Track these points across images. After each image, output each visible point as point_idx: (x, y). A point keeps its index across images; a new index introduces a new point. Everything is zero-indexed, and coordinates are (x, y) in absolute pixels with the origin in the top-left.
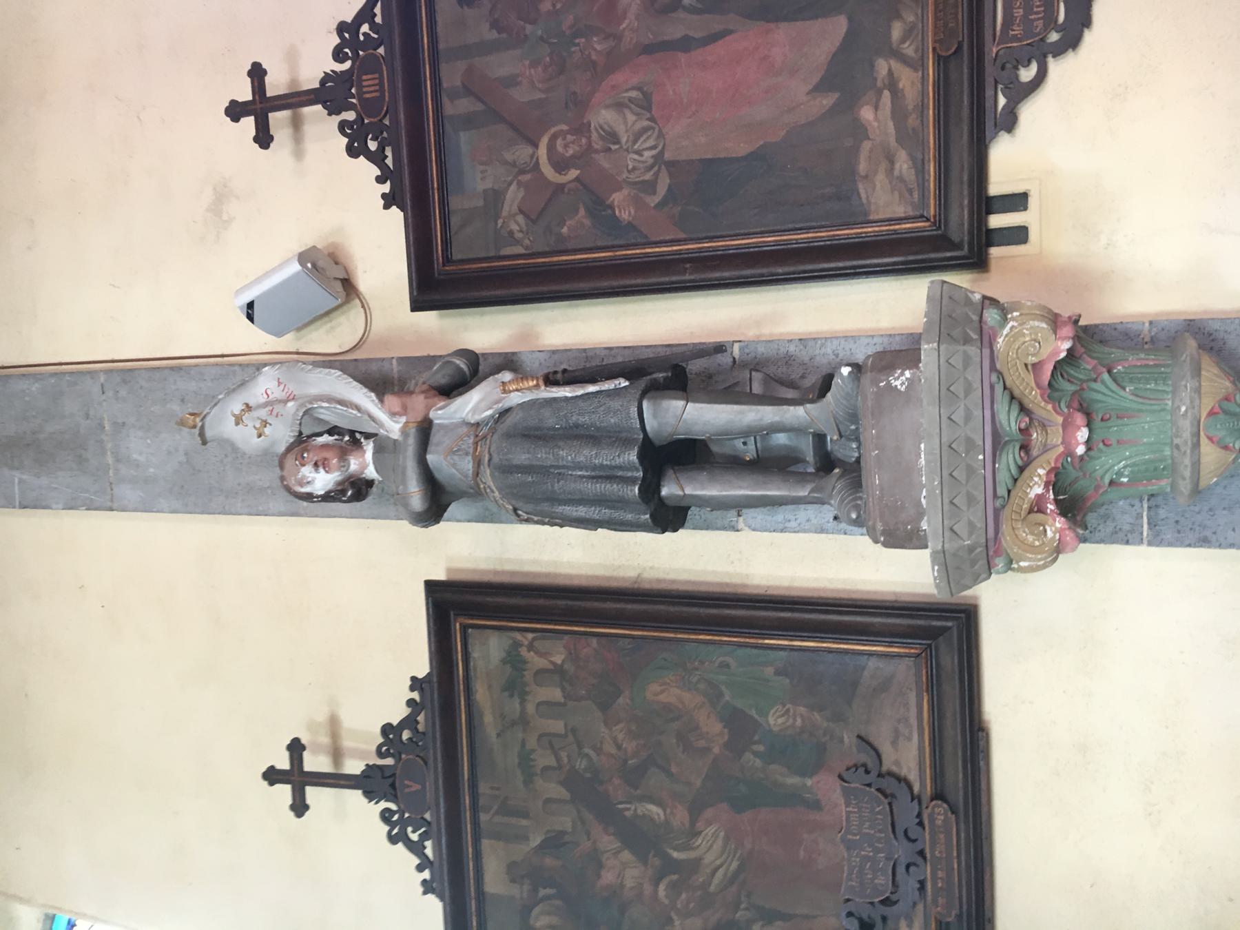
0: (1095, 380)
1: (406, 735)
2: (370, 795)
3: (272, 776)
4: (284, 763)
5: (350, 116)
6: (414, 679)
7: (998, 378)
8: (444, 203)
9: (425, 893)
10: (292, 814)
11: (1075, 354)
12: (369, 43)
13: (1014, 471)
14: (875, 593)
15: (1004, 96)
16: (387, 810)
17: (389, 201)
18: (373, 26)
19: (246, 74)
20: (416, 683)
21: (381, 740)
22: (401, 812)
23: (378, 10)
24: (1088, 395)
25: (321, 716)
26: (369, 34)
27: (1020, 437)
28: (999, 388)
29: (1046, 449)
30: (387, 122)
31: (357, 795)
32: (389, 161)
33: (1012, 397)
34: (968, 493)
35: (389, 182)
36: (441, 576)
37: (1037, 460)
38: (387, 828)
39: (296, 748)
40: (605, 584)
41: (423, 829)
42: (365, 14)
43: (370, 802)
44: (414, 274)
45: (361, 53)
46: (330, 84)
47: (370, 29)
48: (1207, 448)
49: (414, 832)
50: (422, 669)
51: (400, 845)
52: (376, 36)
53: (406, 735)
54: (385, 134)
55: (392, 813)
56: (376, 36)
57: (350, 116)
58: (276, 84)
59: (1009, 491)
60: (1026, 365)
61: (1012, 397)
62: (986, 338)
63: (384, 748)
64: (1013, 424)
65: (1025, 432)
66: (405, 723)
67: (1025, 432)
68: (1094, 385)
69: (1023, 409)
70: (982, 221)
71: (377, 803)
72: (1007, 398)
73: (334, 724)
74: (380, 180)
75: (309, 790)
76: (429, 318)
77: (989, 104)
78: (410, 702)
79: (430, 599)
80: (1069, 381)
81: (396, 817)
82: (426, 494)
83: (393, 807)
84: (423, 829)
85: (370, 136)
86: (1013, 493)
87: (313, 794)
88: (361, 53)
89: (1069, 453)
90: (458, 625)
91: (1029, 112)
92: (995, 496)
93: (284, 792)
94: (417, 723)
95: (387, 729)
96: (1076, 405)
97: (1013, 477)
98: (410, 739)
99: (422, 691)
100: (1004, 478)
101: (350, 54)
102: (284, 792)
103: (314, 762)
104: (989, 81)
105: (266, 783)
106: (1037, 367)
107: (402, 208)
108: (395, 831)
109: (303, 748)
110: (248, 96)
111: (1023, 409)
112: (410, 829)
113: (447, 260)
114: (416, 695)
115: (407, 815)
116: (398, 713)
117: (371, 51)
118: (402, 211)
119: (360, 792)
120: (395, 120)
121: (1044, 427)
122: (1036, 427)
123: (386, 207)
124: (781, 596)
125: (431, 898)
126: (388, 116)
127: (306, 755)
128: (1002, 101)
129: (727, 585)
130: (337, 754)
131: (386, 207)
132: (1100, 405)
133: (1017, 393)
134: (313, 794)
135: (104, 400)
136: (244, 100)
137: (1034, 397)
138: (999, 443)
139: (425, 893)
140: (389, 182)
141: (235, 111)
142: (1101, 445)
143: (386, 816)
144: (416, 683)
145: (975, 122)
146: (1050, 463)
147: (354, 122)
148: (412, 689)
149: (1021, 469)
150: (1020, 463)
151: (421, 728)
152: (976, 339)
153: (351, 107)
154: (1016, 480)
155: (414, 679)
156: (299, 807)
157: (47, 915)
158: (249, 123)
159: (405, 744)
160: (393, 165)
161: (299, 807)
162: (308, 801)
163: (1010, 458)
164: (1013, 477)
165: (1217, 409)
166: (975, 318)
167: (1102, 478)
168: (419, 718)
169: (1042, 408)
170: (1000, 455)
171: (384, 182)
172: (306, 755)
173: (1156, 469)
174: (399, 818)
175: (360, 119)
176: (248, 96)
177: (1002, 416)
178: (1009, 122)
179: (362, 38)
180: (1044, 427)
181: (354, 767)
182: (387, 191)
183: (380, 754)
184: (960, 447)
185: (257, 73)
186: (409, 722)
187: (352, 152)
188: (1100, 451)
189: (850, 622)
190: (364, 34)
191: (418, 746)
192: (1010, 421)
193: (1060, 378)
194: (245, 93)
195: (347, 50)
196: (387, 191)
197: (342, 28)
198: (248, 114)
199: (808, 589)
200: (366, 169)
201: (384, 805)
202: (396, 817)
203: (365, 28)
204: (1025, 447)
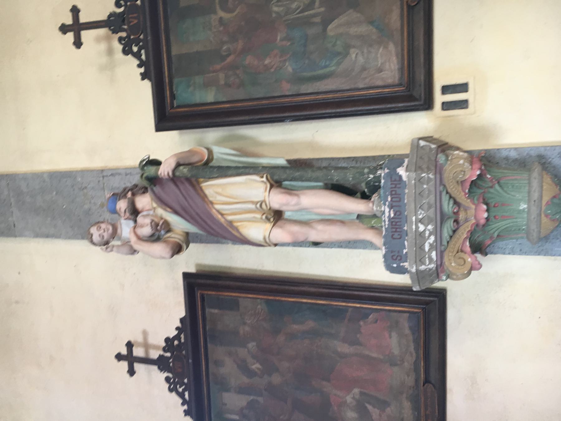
1: (176, 342)
2: (161, 369)
3: (119, 357)
4: (124, 352)
5: (124, 34)
13: (451, 233)
14: (345, 278)
17: (144, 76)
22: (174, 378)
24: (488, 195)
29: (466, 220)
30: (142, 37)
31: (155, 368)
32: (143, 57)
33: (451, 197)
36: (192, 270)
39: (130, 345)
40: (272, 277)
43: (161, 372)
48: (544, 220)
49: (180, 387)
53: (176, 342)
57: (124, 34)
59: (448, 242)
61: (451, 197)
62: (439, 170)
63: (166, 348)
65: (456, 213)
66: (175, 338)
68: (492, 190)
69: (456, 203)
72: (448, 196)
73: (145, 334)
74: (139, 66)
82: (351, 283)
87: (138, 366)
93: (70, 36)
95: (167, 340)
96: (481, 200)
102: (124, 365)
103: (138, 352)
106: (462, 182)
107: (150, 79)
108: (172, 386)
111: (456, 203)
112: (178, 386)
113: (172, 107)
116: (173, 333)
120: (146, 37)
121: (465, 210)
123: (143, 79)
124: (345, 280)
127: (134, 349)
129: (256, 270)
131: (185, 415)
133: (453, 195)
134: (138, 366)
137: (462, 197)
138: (443, 217)
141: (64, 29)
143: (167, 379)
149: (454, 231)
151: (183, 340)
153: (124, 30)
154: (451, 237)
156: (132, 372)
158: (70, 36)
161: (132, 372)
163: (449, 225)
171: (141, 67)
172: (134, 348)
173: (519, 230)
175: (128, 37)
180: (465, 210)
181: (154, 354)
185: (75, 11)
186: (177, 337)
189: (383, 296)
192: (448, 207)
194: (69, 21)
198: (70, 31)
199: (314, 275)
200: (133, 62)
201: (166, 374)
204: (456, 221)
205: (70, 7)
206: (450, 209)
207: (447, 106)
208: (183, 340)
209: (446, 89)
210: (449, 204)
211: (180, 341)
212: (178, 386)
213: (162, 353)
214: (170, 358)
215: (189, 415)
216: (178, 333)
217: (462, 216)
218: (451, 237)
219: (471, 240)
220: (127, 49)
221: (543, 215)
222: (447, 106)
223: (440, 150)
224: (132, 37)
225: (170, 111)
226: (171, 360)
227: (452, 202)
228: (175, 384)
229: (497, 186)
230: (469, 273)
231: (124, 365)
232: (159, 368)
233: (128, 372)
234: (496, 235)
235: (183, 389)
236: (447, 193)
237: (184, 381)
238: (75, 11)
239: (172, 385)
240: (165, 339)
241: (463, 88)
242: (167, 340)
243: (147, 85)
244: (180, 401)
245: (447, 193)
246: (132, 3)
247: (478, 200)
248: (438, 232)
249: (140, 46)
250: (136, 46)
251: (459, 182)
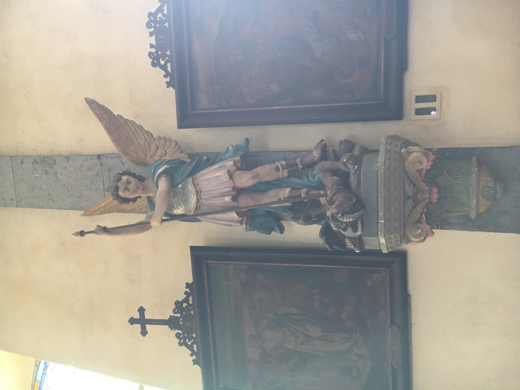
1: (185, 305)
3: (132, 321)
4: (137, 316)
6: (187, 284)
8: (206, 109)
9: (194, 364)
12: (162, 22)
16: (178, 333)
17: (169, 84)
18: (164, 15)
19: (144, 337)
20: (188, 285)
22: (184, 334)
23: (165, 8)
26: (161, 18)
35: (169, 77)
36: (200, 243)
38: (178, 340)
42: (160, 10)
46: (172, 83)
47: (162, 16)
49: (189, 341)
50: (190, 280)
52: (164, 19)
53: (185, 305)
54: (167, 58)
56: (164, 19)
58: (148, 316)
59: (409, 216)
67: (415, 194)
69: (415, 185)
71: (174, 330)
74: (191, 355)
78: (186, 293)
81: (182, 336)
85: (161, 59)
87: (148, 327)
88: (158, 25)
89: (430, 202)
90: (204, 263)
92: (404, 218)
93: (138, 327)
97: (410, 210)
98: (186, 307)
107: (174, 88)
108: (182, 341)
110: (147, 317)
111: (415, 185)
112: (187, 340)
114: (188, 290)
115: (186, 335)
116: (181, 297)
118: (174, 89)
125: (196, 366)
126: (169, 50)
134: (148, 327)
135: (52, 180)
136: (141, 330)
138: (406, 198)
139: (194, 364)
140: (169, 77)
143: (178, 336)
144: (188, 285)
146: (424, 205)
147: (155, 53)
148: (186, 288)
151: (191, 302)
154: (411, 212)
155: (187, 284)
156: (144, 333)
157: (45, 362)
161: (144, 333)
163: (410, 203)
164: (410, 210)
166: (399, 151)
168: (164, 8)
169: (422, 185)
174: (183, 336)
175: (157, 52)
176: (147, 317)
177: (407, 186)
179: (158, 19)
182: (168, 81)
183: (174, 312)
185: (141, 310)
186: (186, 300)
187: (154, 65)
190: (159, 18)
192: (410, 190)
195: (152, 23)
196: (168, 81)
197: (150, 15)
201: (177, 331)
202: (182, 336)
203: (160, 15)
207: (419, 112)
208: (191, 302)
209: (419, 99)
211: (188, 303)
212: (187, 340)
214: (180, 318)
221: (480, 195)
222: (419, 112)
223: (403, 146)
224: (160, 53)
225: (191, 112)
226: (181, 319)
227: (412, 186)
228: (184, 338)
230: (425, 239)
231: (138, 327)
232: (170, 327)
233: (141, 333)
236: (408, 178)
237: (285, 165)
238: (141, 310)
239: (181, 340)
241: (432, 98)
242: (177, 303)
244: (190, 352)
245: (408, 178)
249: (167, 60)
250: (163, 60)
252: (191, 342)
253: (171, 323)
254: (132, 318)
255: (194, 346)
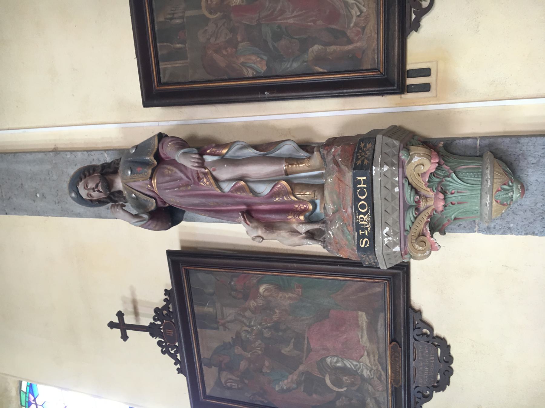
0: (448, 177)
2: (152, 335)
3: (112, 325)
4: (116, 320)
6: (166, 290)
7: (406, 180)
9: (178, 373)
10: (122, 340)
11: (441, 164)
15: (415, 14)
21: (154, 314)
25: (128, 295)
27: (415, 204)
28: (406, 184)
34: (393, 207)
36: (177, 247)
37: (424, 212)
38: (161, 348)
39: (120, 315)
40: (251, 249)
41: (175, 349)
43: (153, 337)
44: (171, 266)
45: (164, 321)
49: (172, 350)
51: (167, 354)
53: (165, 312)
55: (163, 342)
59: (410, 228)
60: (419, 174)
64: (412, 198)
65: (418, 202)
69: (417, 192)
70: (404, 81)
71: (156, 338)
72: (410, 187)
73: (135, 303)
74: (176, 364)
75: (128, 331)
76: (156, 112)
77: (407, 16)
79: (170, 260)
80: (437, 177)
83: (163, 340)
84: (175, 349)
86: (411, 228)
87: (129, 332)
91: (425, 21)
94: (169, 308)
96: (440, 189)
98: (166, 314)
99: (169, 296)
100: (408, 223)
101: (163, 340)
103: (129, 320)
104: (408, 6)
105: (109, 328)
108: (164, 350)
109: (123, 315)
111: (417, 192)
114: (167, 297)
115: (168, 344)
116: (161, 304)
117: (171, 344)
119: (148, 333)
122: (422, 198)
128: (414, 16)
130: (136, 313)
132: (448, 188)
134: (129, 332)
138: (407, 207)
142: (450, 204)
143: (159, 344)
144: (167, 292)
145: (401, 30)
148: (165, 295)
150: (415, 216)
151: (171, 310)
152: (396, 164)
154: (413, 223)
155: (166, 290)
156: (125, 337)
159: (163, 315)
160: (181, 359)
161: (125, 337)
162: (128, 335)
163: (411, 214)
165: (500, 189)
167: (451, 216)
170: (406, 213)
178: (416, 26)
181: (146, 321)
183: (154, 319)
184: (389, 186)
186: (166, 307)
188: (449, 206)
191: (170, 317)
192: (410, 198)
193: (433, 176)
201: (158, 339)
202: (164, 344)
204: (417, 209)
205: (128, 340)
206: (412, 201)
210: (411, 195)
213: (152, 321)
214: (160, 325)
215: (182, 373)
216: (166, 304)
217: (422, 205)
218: (415, 218)
219: (431, 225)
220: (165, 350)
229: (454, 175)
234: (453, 217)
235: (174, 351)
236: (409, 184)
240: (154, 310)
242: (157, 310)
243: (182, 380)
245: (409, 184)
246: (167, 321)
247: (437, 189)
248: (403, 218)
251: (420, 175)
252: (174, 350)
253: (152, 330)
254: (111, 322)
255: (177, 355)
